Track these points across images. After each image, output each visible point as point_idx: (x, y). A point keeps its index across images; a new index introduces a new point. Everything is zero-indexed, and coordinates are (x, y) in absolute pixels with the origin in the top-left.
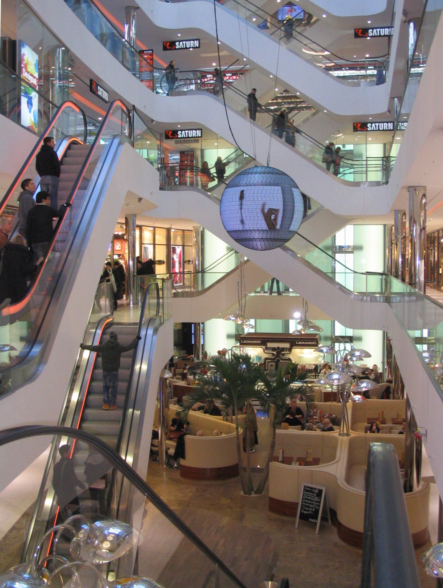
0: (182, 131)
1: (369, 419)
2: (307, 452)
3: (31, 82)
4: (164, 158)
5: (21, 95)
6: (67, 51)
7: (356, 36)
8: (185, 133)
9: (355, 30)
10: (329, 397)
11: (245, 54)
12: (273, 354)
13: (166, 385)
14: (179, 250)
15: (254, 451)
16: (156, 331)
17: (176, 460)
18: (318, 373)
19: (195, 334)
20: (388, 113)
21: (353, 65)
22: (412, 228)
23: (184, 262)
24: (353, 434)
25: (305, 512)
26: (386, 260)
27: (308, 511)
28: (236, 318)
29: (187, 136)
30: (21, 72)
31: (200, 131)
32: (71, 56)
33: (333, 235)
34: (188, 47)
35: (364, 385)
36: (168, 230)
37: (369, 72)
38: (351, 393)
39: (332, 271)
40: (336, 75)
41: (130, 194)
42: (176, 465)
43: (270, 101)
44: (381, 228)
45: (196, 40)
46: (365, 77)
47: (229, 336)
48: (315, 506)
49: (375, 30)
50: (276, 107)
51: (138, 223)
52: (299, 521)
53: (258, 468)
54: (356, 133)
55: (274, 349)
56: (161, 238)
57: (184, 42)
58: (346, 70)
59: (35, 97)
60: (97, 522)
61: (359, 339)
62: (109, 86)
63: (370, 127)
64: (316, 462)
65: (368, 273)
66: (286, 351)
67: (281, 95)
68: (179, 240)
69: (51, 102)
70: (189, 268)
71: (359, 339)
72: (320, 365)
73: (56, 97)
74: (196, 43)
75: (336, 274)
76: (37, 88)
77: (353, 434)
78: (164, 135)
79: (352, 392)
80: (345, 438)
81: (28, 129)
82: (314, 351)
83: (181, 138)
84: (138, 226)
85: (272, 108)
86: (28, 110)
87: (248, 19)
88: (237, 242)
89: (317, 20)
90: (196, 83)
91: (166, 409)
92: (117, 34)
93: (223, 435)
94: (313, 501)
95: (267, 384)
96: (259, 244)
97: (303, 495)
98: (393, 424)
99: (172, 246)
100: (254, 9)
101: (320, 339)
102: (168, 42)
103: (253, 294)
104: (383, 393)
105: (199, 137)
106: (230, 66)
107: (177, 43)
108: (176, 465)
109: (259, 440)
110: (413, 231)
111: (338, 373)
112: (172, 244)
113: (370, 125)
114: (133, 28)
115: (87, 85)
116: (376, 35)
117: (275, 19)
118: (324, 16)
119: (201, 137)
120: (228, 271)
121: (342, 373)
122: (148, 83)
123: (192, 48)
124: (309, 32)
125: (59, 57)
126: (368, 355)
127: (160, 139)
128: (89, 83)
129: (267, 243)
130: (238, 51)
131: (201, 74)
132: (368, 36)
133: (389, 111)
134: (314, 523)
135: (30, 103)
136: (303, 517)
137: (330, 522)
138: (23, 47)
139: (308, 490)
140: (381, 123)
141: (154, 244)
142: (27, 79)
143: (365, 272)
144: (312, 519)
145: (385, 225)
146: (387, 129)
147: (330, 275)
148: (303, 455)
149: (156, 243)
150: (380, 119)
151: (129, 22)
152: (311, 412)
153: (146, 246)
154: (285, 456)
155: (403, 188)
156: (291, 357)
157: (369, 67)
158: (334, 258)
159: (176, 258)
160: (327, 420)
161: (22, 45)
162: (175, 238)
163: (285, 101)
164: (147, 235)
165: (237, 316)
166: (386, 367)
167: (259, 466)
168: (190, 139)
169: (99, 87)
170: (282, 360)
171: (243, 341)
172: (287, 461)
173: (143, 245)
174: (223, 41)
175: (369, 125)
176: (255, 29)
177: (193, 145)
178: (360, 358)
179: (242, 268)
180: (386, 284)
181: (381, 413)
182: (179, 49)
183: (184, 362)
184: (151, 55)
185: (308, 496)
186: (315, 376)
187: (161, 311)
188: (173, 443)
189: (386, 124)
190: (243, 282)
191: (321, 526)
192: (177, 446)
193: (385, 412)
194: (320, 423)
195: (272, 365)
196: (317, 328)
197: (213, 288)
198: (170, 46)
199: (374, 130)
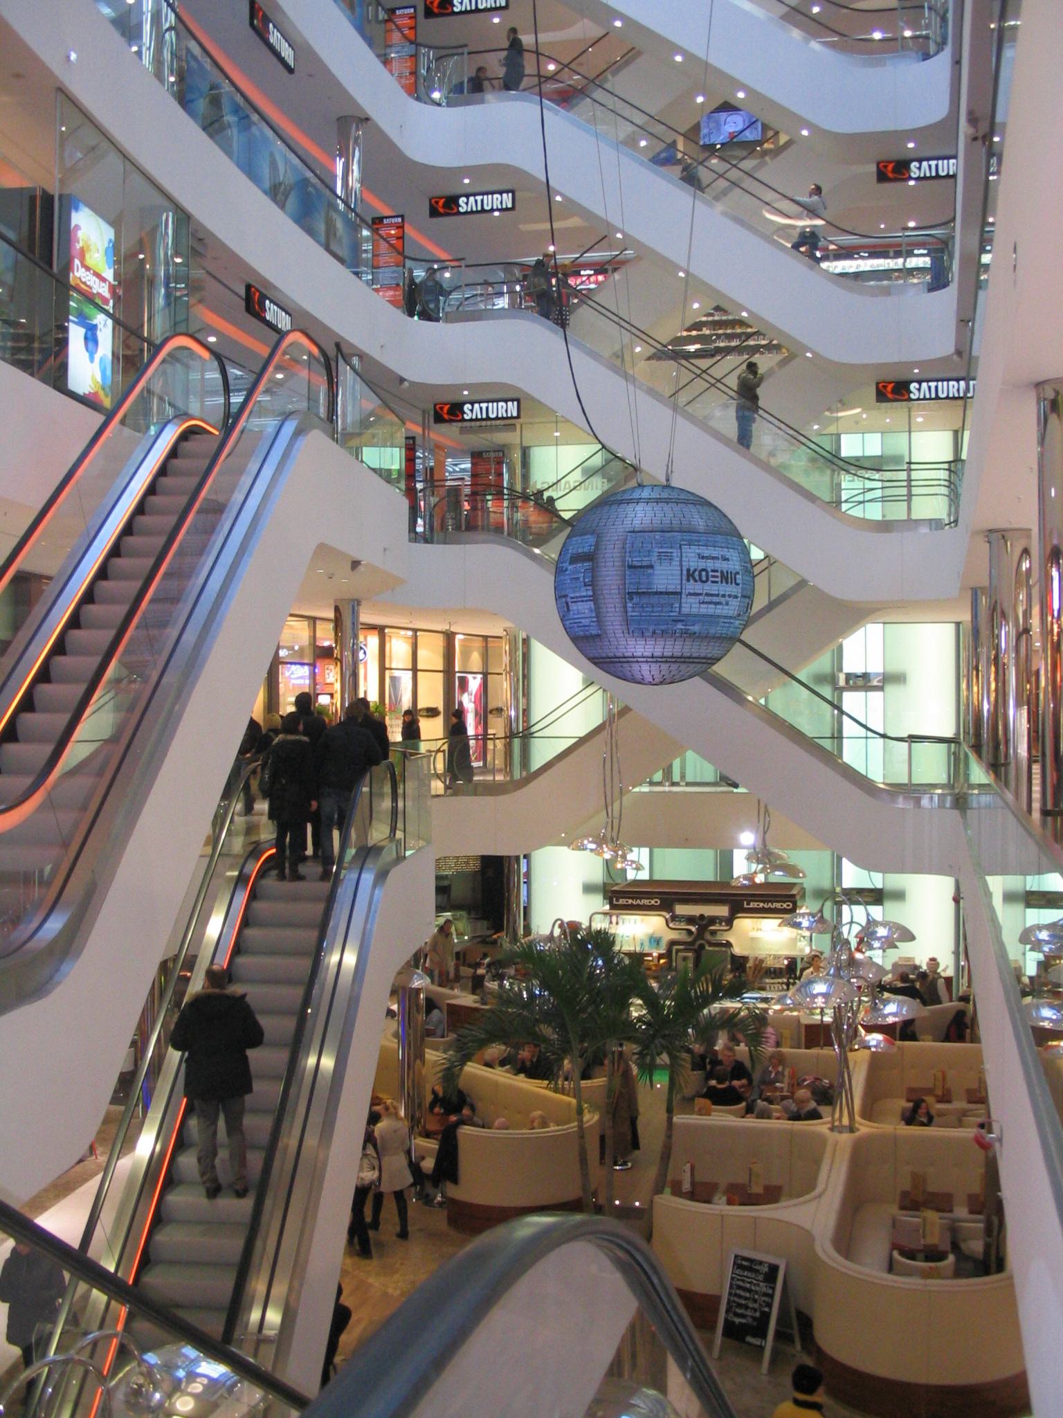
0: (472, 404)
1: (911, 1090)
2: (750, 1170)
3: (95, 292)
4: (432, 469)
5: (68, 321)
6: (184, 218)
7: (882, 177)
8: (481, 409)
9: (878, 164)
10: (816, 1035)
11: (615, 220)
12: (689, 932)
13: (418, 1005)
14: (474, 683)
15: (630, 1165)
16: (382, 876)
17: (436, 1186)
18: (796, 978)
19: (528, 883)
20: (955, 357)
21: (875, 246)
22: (996, 632)
23: (485, 713)
24: (865, 1128)
25: (737, 1320)
26: (962, 708)
27: (743, 1316)
28: (599, 845)
29: (484, 416)
30: (68, 267)
31: (515, 403)
32: (197, 231)
33: (834, 646)
34: (486, 208)
35: (891, 1008)
36: (449, 637)
37: (913, 262)
38: (860, 1027)
39: (833, 734)
40: (838, 271)
41: (323, 551)
42: (439, 1199)
43: (685, 334)
44: (951, 628)
45: (507, 192)
46: (911, 272)
47: (589, 889)
48: (760, 1305)
49: (925, 164)
50: (698, 346)
51: (366, 617)
52: (723, 1343)
53: (637, 1208)
54: (884, 405)
55: (691, 920)
56: (431, 656)
57: (479, 198)
58: (862, 258)
59: (105, 324)
60: (150, 1354)
61: (899, 896)
62: (286, 296)
63: (917, 392)
64: (772, 1195)
65: (913, 739)
66: (720, 924)
67: (710, 319)
68: (476, 660)
69: (144, 340)
70: (497, 727)
71: (899, 896)
72: (802, 959)
73: (156, 324)
74: (507, 200)
75: (844, 740)
76: (110, 307)
77: (865, 1128)
78: (432, 413)
79: (862, 1025)
80: (846, 1138)
81: (88, 401)
82: (780, 925)
83: (471, 420)
84: (373, 627)
85: (692, 348)
86: (87, 354)
87: (631, 142)
88: (595, 664)
89: (789, 143)
90: (511, 292)
91: (418, 1062)
92: (314, 180)
93: (553, 1127)
94: (757, 1292)
95: (652, 1002)
96: (646, 670)
97: (732, 1279)
98: (970, 1102)
99: (458, 675)
100: (639, 119)
101: (803, 897)
102: (441, 198)
103: (645, 789)
104: (949, 1027)
105: (512, 418)
106: (585, 252)
107: (462, 200)
108: (439, 1199)
109: (643, 1142)
110: (999, 637)
111: (826, 981)
112: (457, 669)
113: (916, 385)
114: (355, 167)
115: (240, 296)
116: (928, 175)
117: (693, 145)
118: (805, 133)
119: (518, 417)
120: (582, 734)
121: (836, 980)
122: (391, 293)
123: (498, 210)
124: (770, 171)
125: (167, 233)
126: (908, 936)
127: (424, 424)
128: (242, 292)
129: (664, 666)
130: (596, 212)
131: (521, 271)
132: (910, 178)
133: (959, 353)
134: (757, 1346)
135: (91, 339)
136: (732, 1331)
137: (798, 1346)
138: (77, 209)
139: (744, 1265)
140: (943, 380)
141: (415, 670)
142: (84, 283)
143: (906, 736)
144: (754, 1336)
145: (958, 624)
146: (956, 395)
147: (827, 744)
148: (742, 1179)
149: (419, 668)
150: (937, 371)
151: (345, 153)
152: (771, 1072)
153: (396, 673)
154: (698, 1179)
155: (975, 533)
156: (732, 940)
157: (916, 252)
158: (839, 708)
159: (468, 702)
160: (803, 1093)
161: (69, 204)
162: (466, 655)
163: (720, 332)
164: (399, 648)
165: (600, 841)
166: (962, 963)
167: (637, 1204)
168: (494, 422)
169: (267, 302)
170: (711, 944)
171: (617, 900)
172: (701, 1193)
173: (387, 672)
174: (568, 194)
175: (914, 386)
176: (642, 164)
177: (501, 438)
178: (889, 944)
179: (614, 726)
180: (957, 765)
181: (939, 1075)
182: (466, 213)
183: (484, 949)
184: (400, 227)
185: (743, 1281)
186: (788, 984)
187: (400, 825)
188: (433, 1145)
189: (955, 383)
190: (615, 760)
191: (775, 1353)
192: (440, 1151)
193: (950, 1074)
194: (791, 1101)
195: (685, 959)
196: (790, 869)
197: (549, 772)
198: (445, 206)
199: (925, 399)
